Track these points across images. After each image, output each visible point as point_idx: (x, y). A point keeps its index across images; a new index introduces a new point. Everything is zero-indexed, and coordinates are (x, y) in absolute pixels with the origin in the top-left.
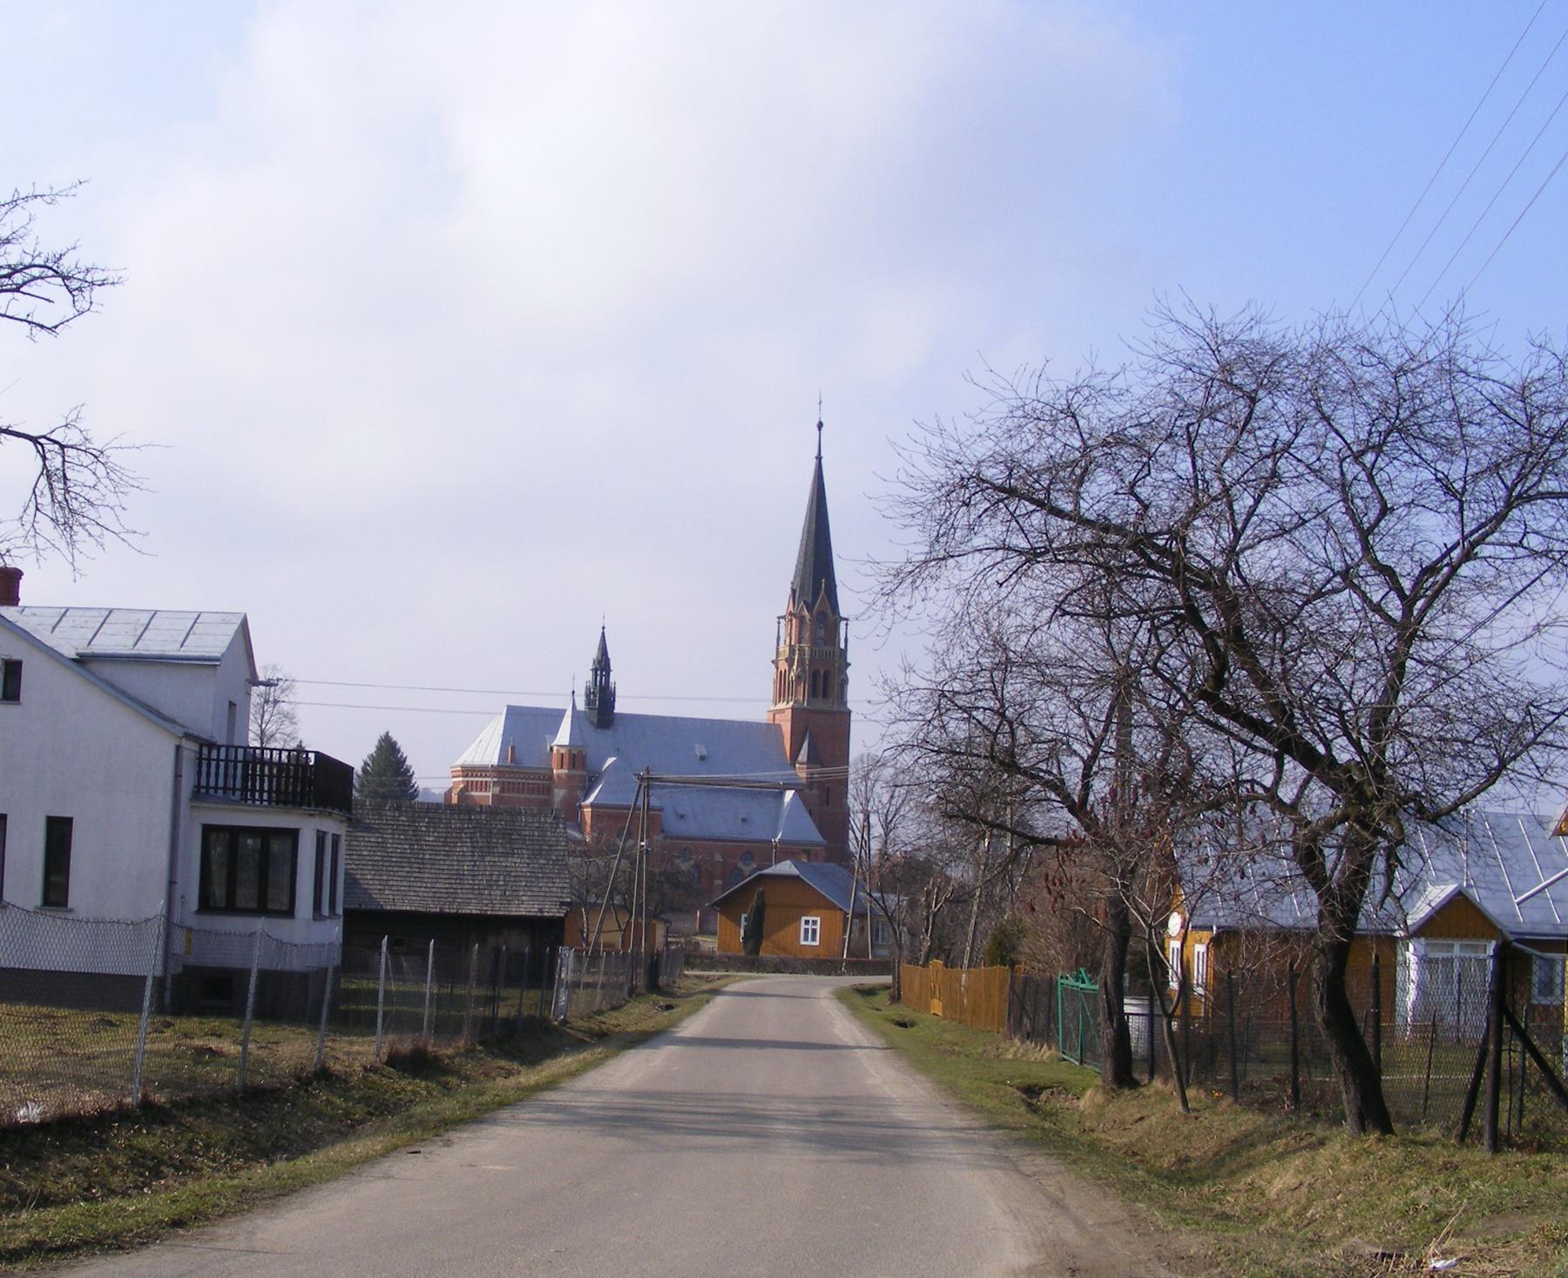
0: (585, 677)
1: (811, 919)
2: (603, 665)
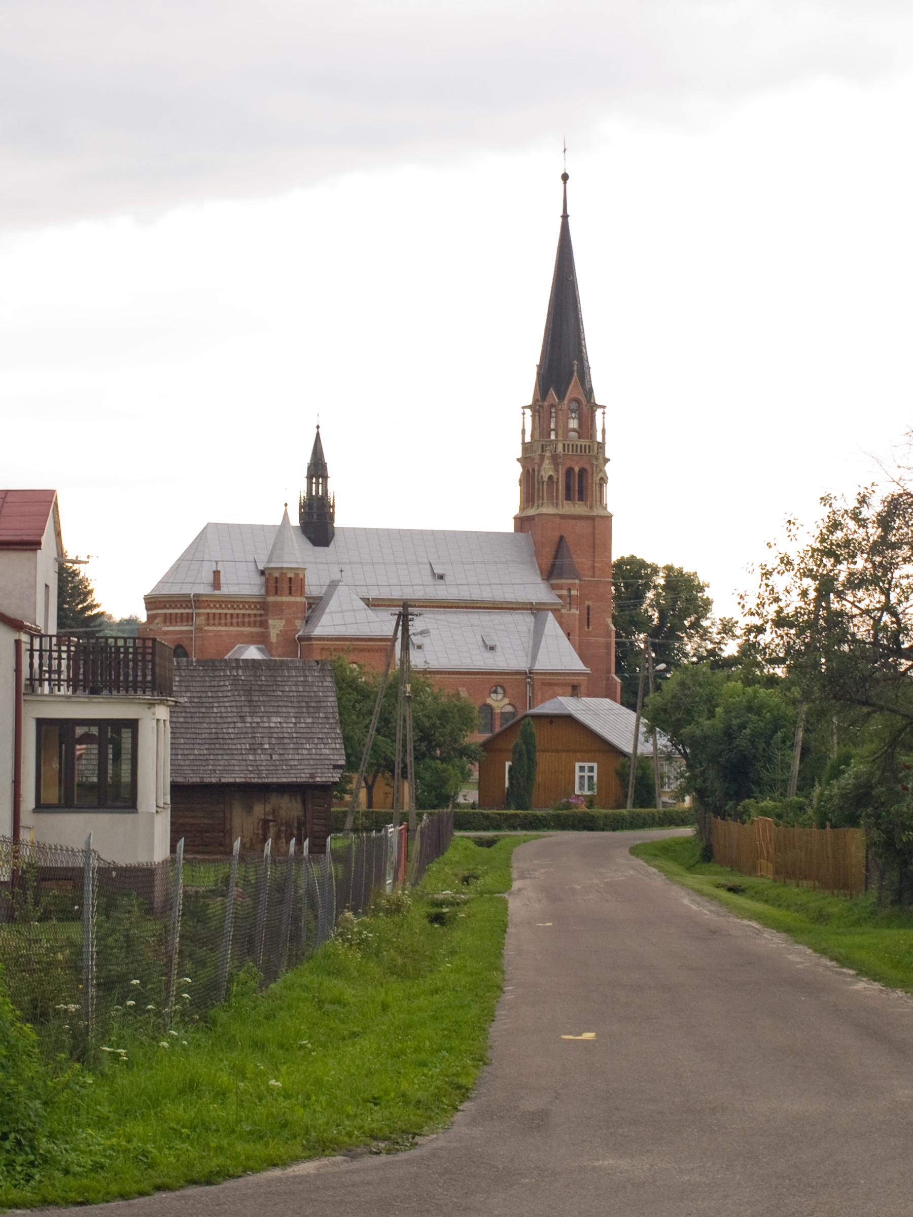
0: (296, 488)
1: (587, 765)
2: (317, 469)
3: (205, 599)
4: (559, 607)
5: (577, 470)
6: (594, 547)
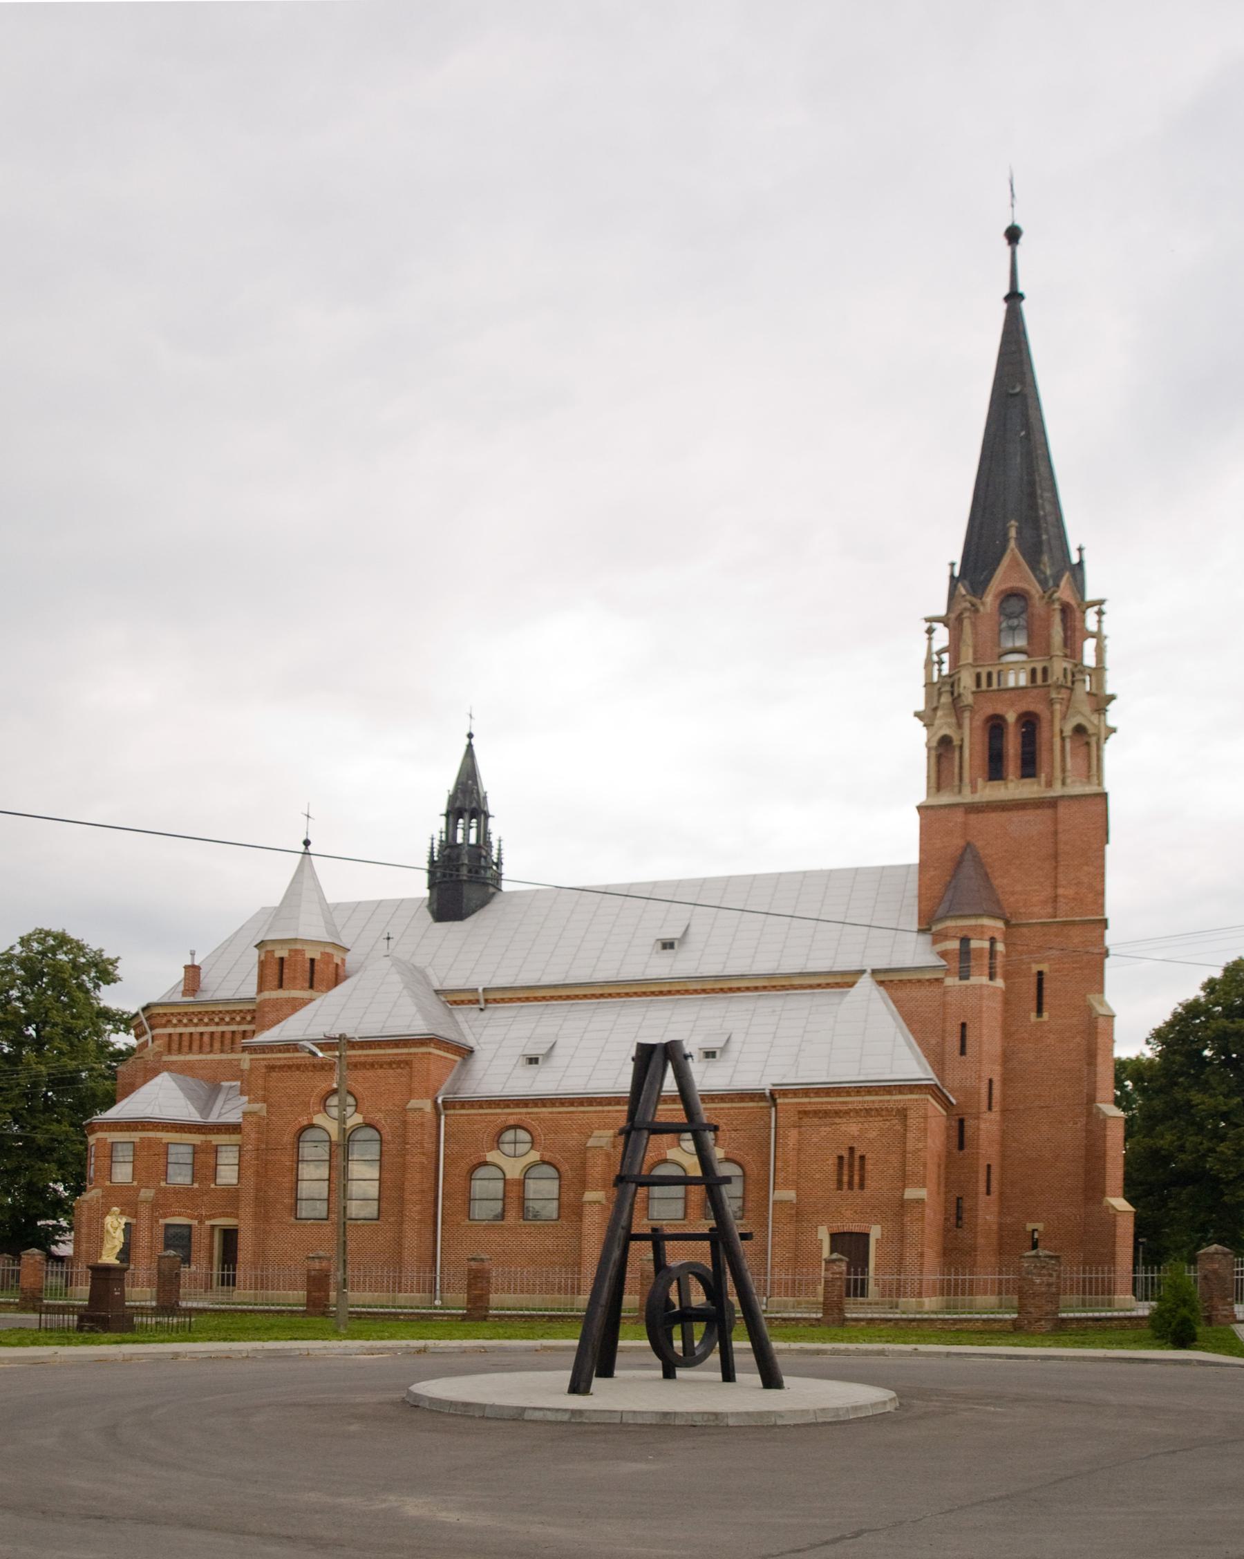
3: (161, 1011)
4: (940, 975)
5: (1011, 717)
6: (1055, 856)
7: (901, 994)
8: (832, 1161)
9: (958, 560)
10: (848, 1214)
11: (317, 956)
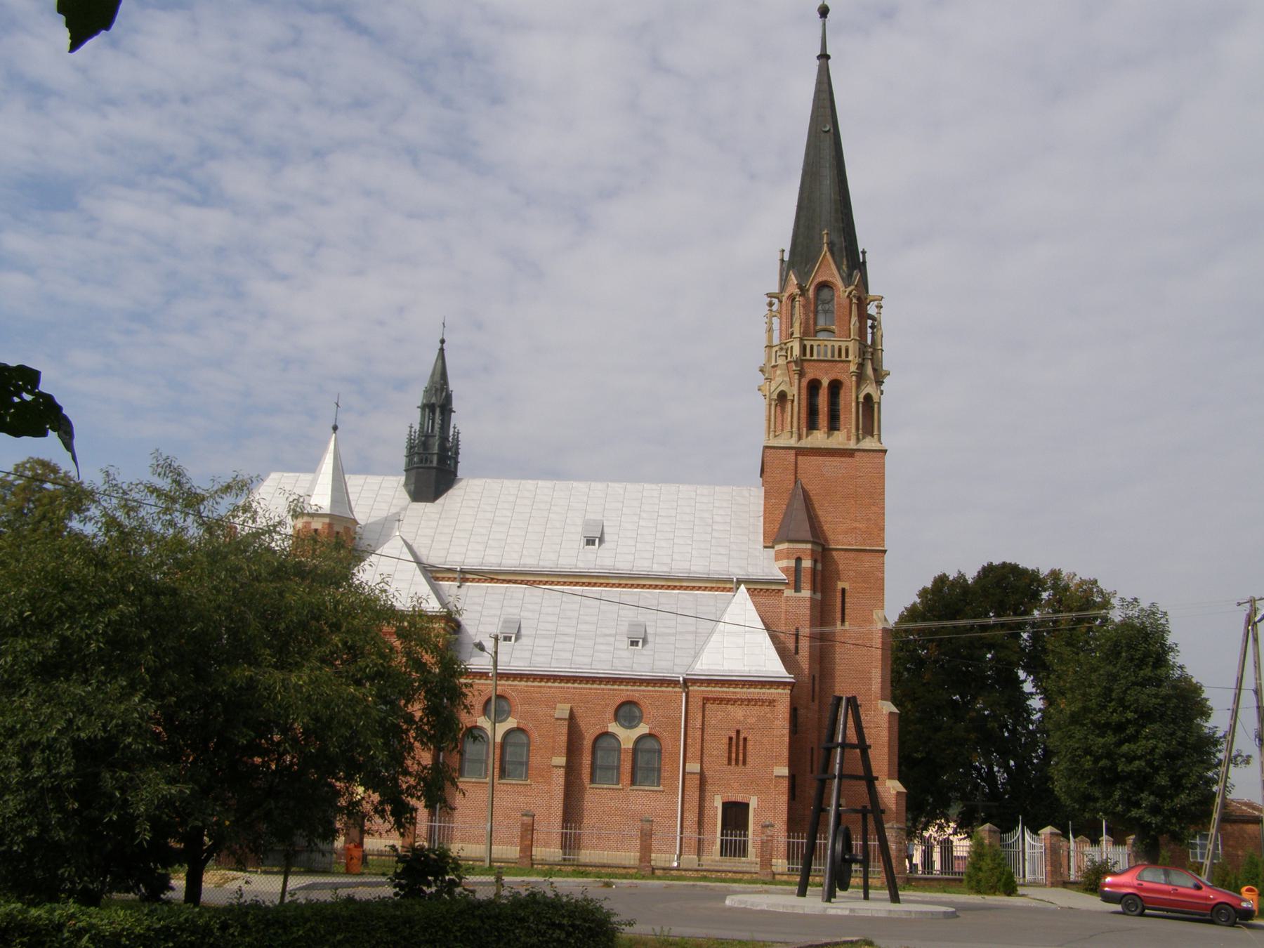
5: (825, 382)
7: (762, 600)
8: (726, 741)
9: (788, 248)
10: (735, 786)
11: (341, 530)
